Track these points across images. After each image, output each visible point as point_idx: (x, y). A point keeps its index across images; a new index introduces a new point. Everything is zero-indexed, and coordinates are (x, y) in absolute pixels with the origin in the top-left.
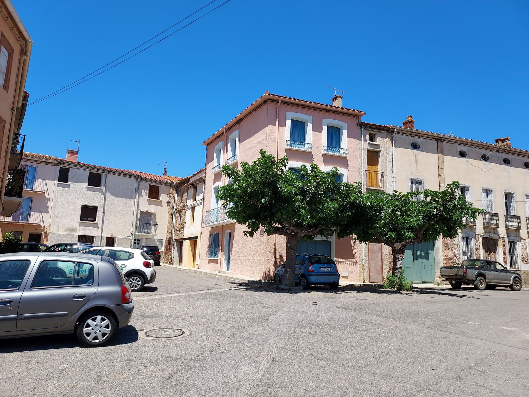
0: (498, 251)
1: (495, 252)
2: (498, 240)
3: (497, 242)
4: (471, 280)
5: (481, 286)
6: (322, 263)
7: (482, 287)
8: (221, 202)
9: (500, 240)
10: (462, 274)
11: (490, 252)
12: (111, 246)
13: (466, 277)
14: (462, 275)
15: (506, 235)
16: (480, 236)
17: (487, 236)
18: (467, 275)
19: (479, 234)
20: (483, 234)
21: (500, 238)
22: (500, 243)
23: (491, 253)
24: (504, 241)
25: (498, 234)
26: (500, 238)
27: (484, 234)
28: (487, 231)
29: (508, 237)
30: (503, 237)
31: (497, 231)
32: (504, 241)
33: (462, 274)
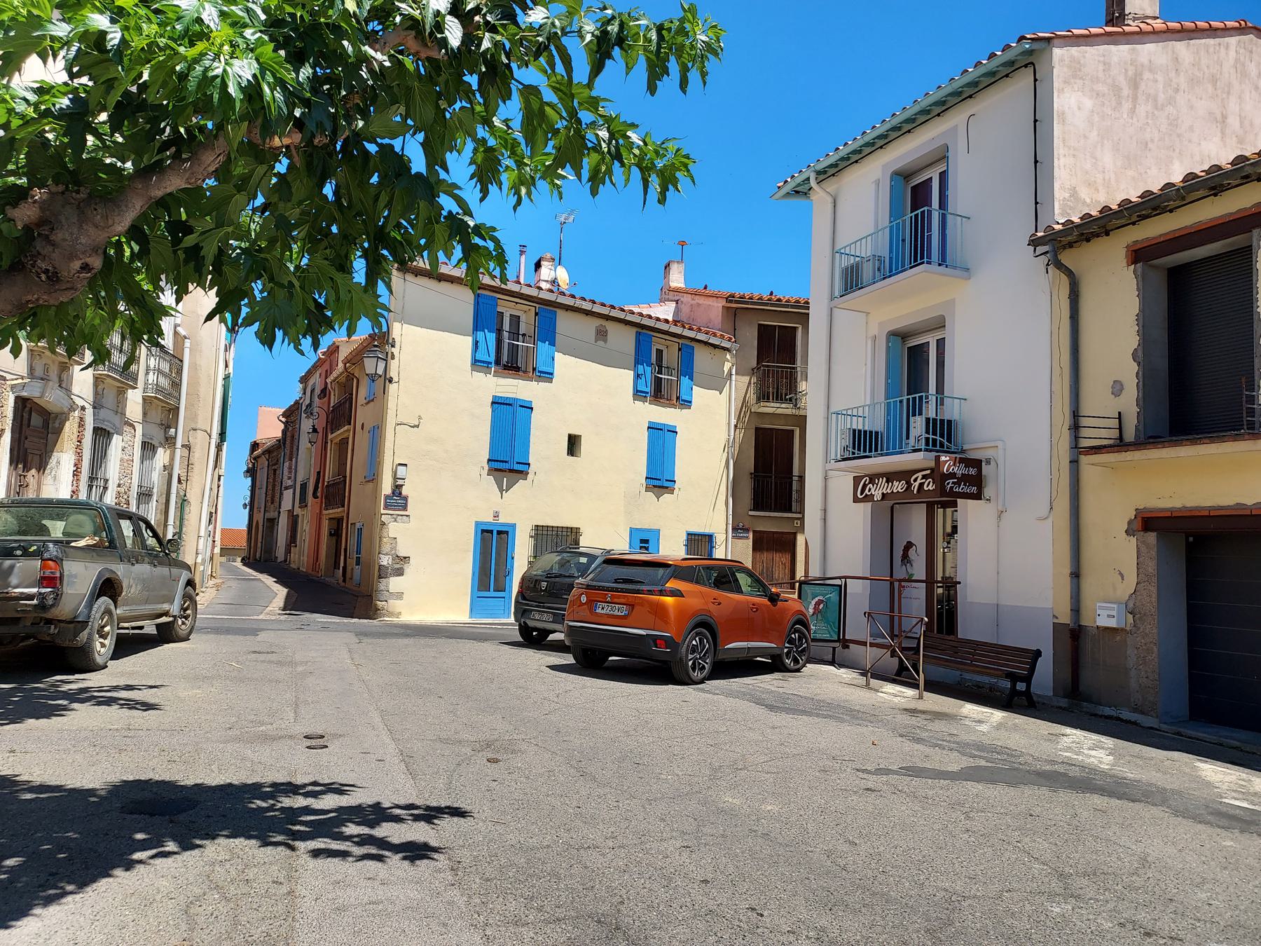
0: (58, 463)
1: (42, 467)
2: (62, 418)
3: (57, 425)
4: (60, 621)
5: (183, 623)
6: (5, 642)
7: (183, 627)
8: (530, 12)
9: (71, 418)
10: (35, 590)
11: (27, 468)
12: (1188, 626)
13: (53, 606)
14: (30, 597)
15: (91, 398)
16: (13, 387)
17: (32, 392)
18: (58, 597)
19: (8, 376)
20: (20, 381)
21: (73, 407)
22: (70, 428)
23: (27, 472)
24: (82, 422)
25: (68, 391)
26: (73, 407)
27: (26, 381)
28: (39, 371)
29: (94, 408)
30: (83, 408)
31: (70, 378)
32: (82, 422)
33: (35, 590)
